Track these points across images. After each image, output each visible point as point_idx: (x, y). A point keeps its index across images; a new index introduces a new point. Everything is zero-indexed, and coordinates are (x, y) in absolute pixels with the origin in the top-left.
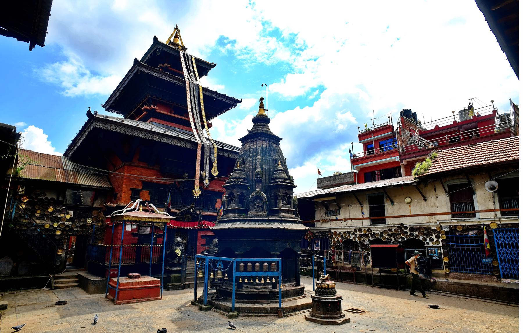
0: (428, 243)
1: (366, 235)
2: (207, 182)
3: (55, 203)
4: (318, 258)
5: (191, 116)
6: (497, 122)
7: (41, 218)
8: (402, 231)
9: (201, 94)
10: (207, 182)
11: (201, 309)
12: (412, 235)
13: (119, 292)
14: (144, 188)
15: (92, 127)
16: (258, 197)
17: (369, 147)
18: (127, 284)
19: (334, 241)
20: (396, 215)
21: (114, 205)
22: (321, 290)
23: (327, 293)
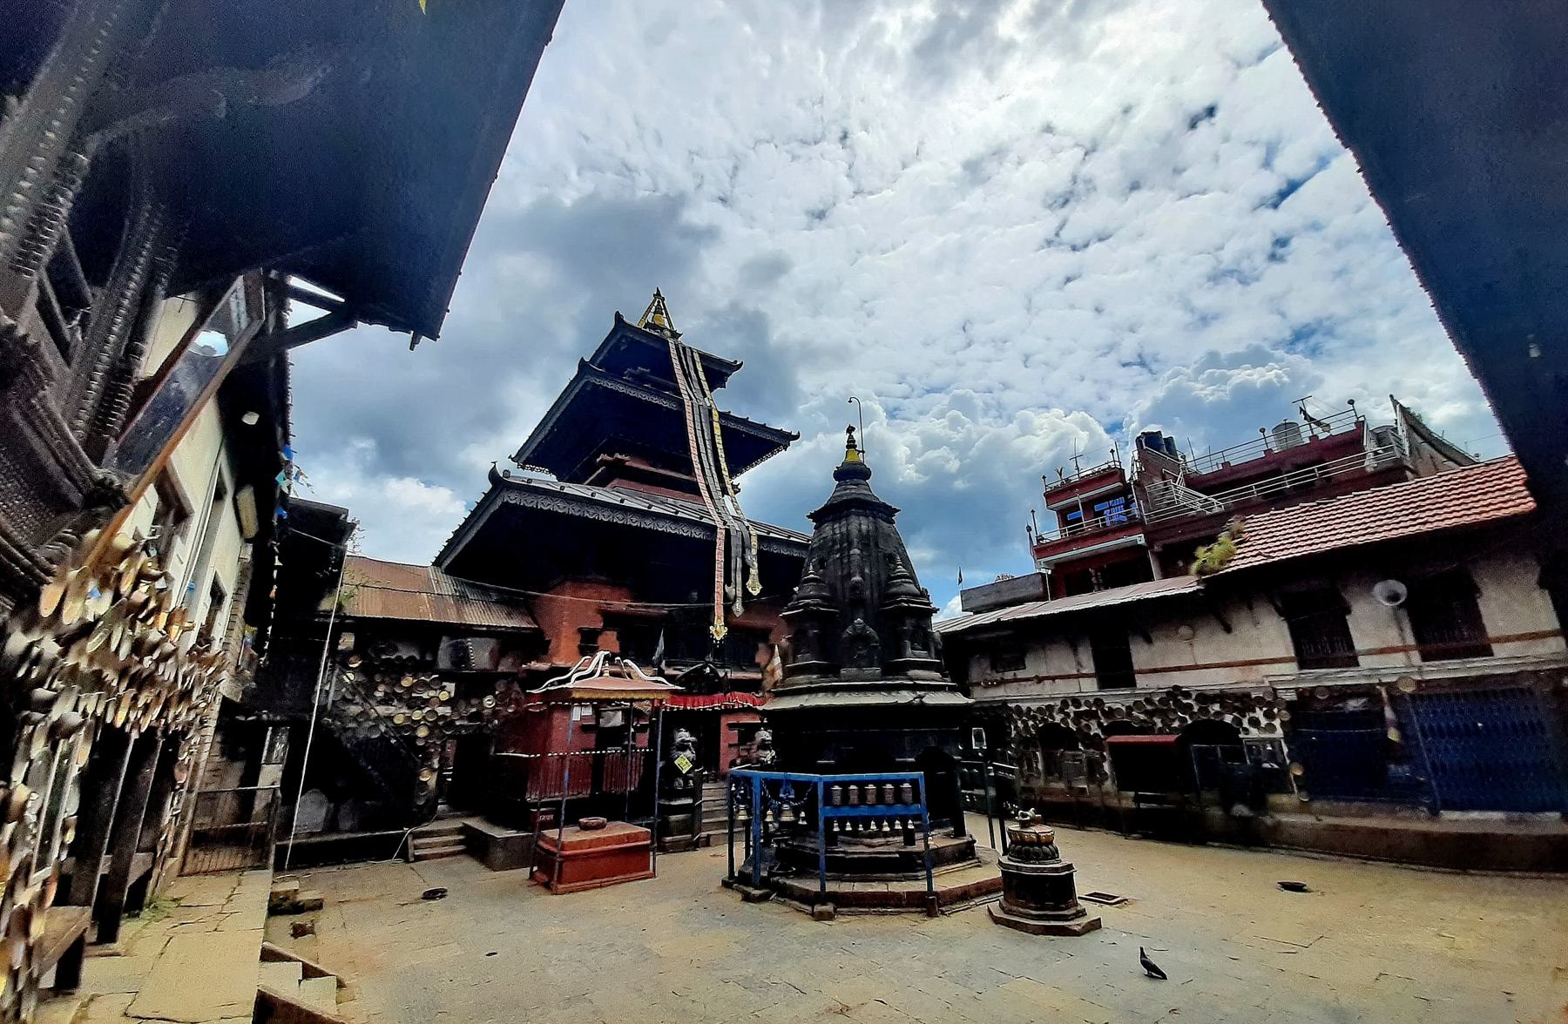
0: (1246, 731)
1: (1090, 715)
2: (738, 608)
3: (416, 667)
4: (997, 769)
5: (698, 471)
6: (1370, 445)
7: (386, 701)
8: (1177, 702)
9: (716, 425)
10: (738, 608)
11: (747, 898)
12: (1204, 710)
13: (561, 864)
14: (605, 628)
15: (499, 502)
16: (860, 638)
17: (1070, 517)
18: (580, 844)
19: (1016, 727)
20: (1160, 666)
21: (544, 666)
22: (1022, 848)
23: (1037, 854)
